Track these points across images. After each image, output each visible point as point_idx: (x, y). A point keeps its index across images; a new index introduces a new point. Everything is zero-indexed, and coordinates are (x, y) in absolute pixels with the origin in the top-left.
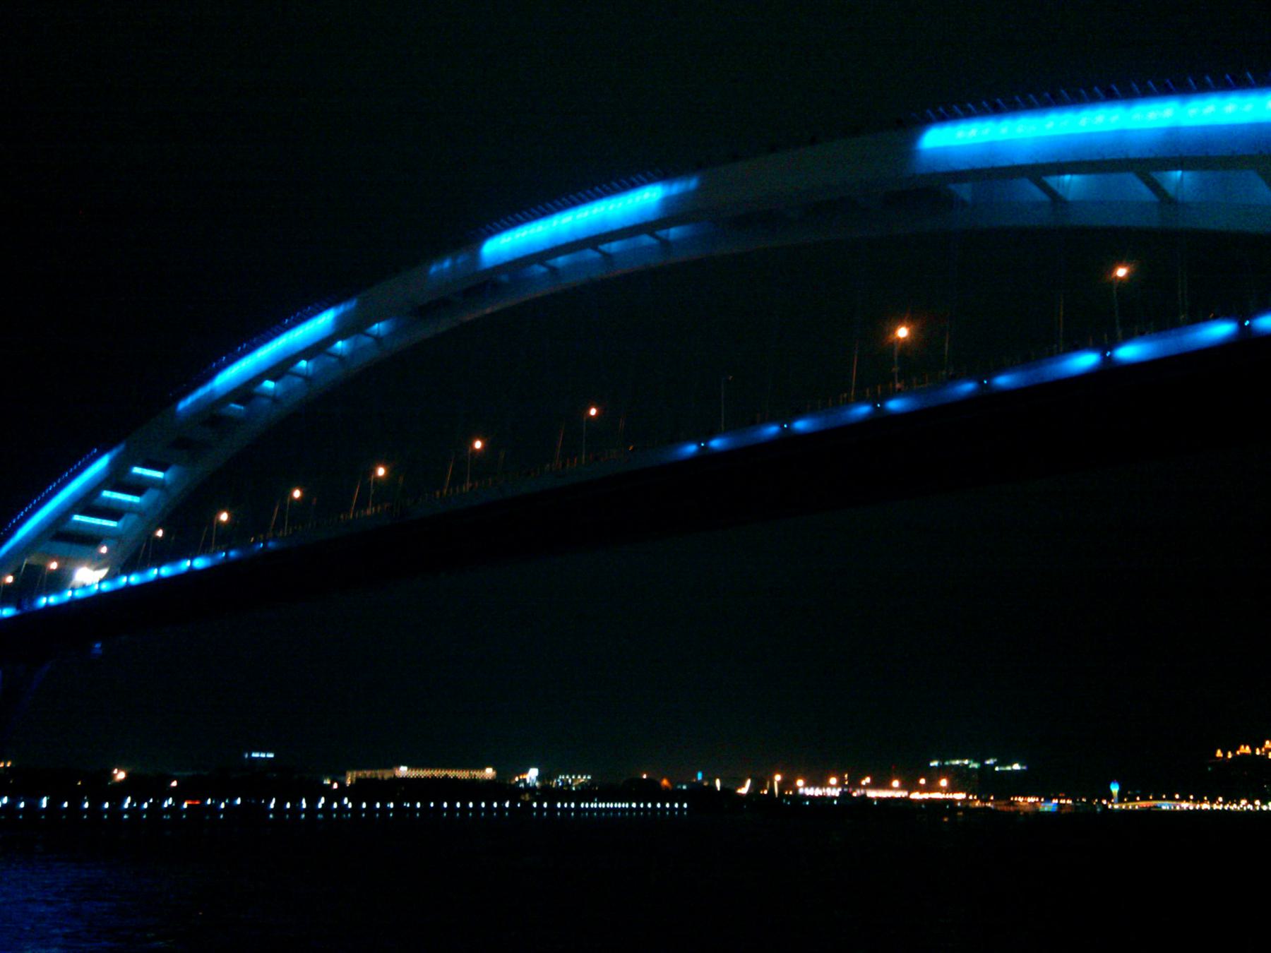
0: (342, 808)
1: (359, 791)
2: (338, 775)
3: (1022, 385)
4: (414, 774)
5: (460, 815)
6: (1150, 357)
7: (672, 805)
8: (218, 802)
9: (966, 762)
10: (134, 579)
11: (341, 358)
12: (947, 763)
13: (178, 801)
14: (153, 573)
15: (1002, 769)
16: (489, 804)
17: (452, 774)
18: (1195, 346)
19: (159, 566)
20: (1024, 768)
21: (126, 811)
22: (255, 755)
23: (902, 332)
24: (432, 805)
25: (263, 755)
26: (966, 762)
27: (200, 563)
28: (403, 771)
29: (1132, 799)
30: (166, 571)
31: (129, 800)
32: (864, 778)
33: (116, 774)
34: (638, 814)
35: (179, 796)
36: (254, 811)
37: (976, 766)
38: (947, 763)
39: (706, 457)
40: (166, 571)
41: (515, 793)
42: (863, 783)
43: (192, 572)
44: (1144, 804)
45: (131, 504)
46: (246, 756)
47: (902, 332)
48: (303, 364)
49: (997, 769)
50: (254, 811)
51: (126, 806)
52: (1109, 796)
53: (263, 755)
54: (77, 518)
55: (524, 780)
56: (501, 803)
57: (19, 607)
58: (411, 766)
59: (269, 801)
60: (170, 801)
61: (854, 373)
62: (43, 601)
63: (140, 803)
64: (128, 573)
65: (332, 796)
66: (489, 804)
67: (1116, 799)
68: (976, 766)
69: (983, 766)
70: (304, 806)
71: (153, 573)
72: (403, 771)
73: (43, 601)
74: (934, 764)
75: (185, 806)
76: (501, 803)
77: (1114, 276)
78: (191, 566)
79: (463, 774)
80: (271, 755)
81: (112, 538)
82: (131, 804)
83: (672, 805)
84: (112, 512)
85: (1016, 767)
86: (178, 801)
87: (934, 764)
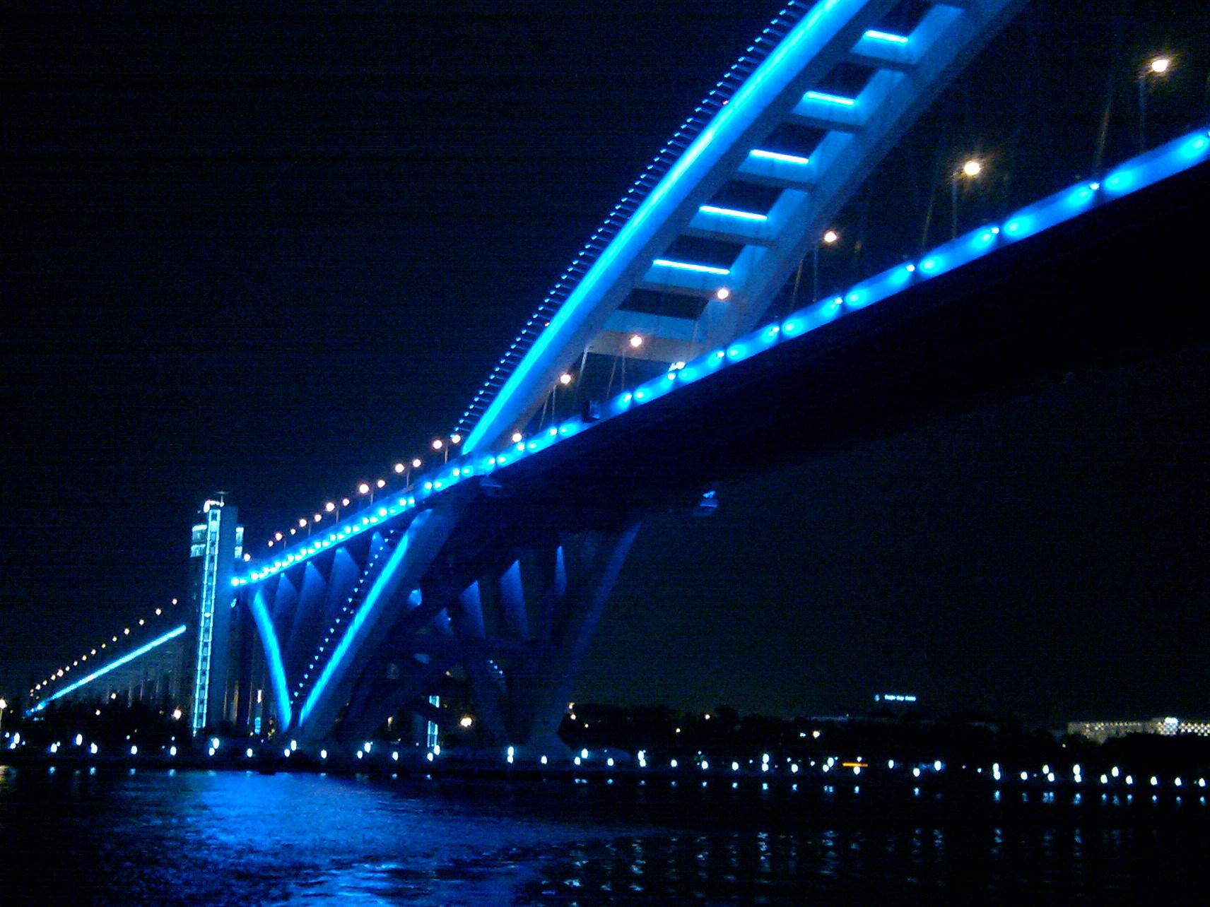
6: (948, 270)
8: (627, 756)
10: (794, 327)
14: (830, 309)
16: (1166, 781)
19: (632, 390)
23: (972, 169)
24: (964, 767)
25: (900, 698)
30: (859, 297)
33: (834, 758)
40: (859, 297)
43: (1005, 251)
45: (893, 49)
46: (877, 698)
47: (972, 169)
53: (900, 698)
56: (1189, 779)
57: (586, 418)
58: (1183, 716)
60: (585, 753)
62: (624, 401)
66: (1166, 781)
70: (997, 775)
71: (830, 309)
72: (1170, 725)
73: (624, 401)
76: (1189, 779)
77: (990, 157)
78: (780, 334)
80: (913, 699)
81: (757, 241)
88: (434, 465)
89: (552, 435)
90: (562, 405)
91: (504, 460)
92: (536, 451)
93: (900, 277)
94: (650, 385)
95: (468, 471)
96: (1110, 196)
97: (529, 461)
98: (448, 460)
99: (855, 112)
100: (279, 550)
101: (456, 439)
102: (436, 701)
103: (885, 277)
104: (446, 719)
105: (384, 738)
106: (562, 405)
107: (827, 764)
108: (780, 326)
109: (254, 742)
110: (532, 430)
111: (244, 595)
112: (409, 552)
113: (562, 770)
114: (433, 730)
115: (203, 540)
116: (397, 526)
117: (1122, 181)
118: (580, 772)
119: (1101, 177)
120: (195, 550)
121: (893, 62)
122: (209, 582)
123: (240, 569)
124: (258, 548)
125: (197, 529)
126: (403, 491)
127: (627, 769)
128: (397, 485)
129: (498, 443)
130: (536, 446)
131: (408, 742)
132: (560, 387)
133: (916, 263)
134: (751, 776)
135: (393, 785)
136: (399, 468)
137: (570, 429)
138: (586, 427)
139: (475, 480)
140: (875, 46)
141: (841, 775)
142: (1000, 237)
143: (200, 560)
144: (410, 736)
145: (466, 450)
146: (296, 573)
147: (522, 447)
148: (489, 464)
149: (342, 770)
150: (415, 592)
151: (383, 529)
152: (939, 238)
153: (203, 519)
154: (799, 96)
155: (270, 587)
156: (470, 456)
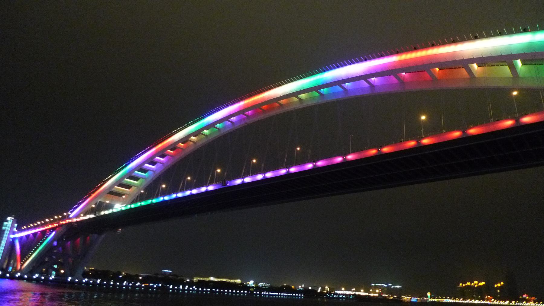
0: (193, 290)
1: (200, 284)
2: (192, 278)
3: (433, 143)
4: (216, 280)
5: (90, 286)
7: (236, 291)
9: (383, 284)
11: (206, 136)
12: (377, 285)
13: (141, 283)
15: (394, 287)
17: (228, 280)
18: (501, 128)
19: (141, 202)
20: (401, 287)
21: (124, 286)
22: (165, 271)
26: (464, 285)
27: (211, 188)
28: (212, 279)
29: (434, 298)
30: (194, 191)
31: (125, 282)
32: (124, 283)
34: (153, 289)
35: (142, 282)
36: (165, 289)
37: (386, 286)
38: (377, 285)
39: (243, 184)
41: (248, 288)
42: (352, 290)
43: (207, 192)
44: (454, 301)
48: (193, 138)
49: (392, 287)
50: (165, 289)
51: (124, 284)
52: (427, 297)
54: (136, 172)
55: (249, 284)
57: (95, 215)
58: (215, 277)
59: (170, 286)
61: (209, 179)
62: (102, 213)
63: (129, 284)
64: (131, 204)
65: (191, 284)
67: (429, 297)
68: (386, 286)
69: (388, 286)
74: (373, 285)
75: (143, 285)
79: (232, 281)
82: (126, 284)
83: (236, 291)
84: (128, 186)
85: (398, 287)
86: (141, 283)
87: (373, 285)
88: (64, 218)
89: (88, 217)
90: (92, 211)
91: (78, 220)
92: (143, 205)
93: (174, 196)
94: (169, 196)
95: (70, 221)
96: (267, 177)
97: (83, 221)
98: (209, 183)
99: (154, 168)
100: (25, 230)
101: (69, 213)
102: (56, 266)
103: (234, 181)
104: (57, 271)
105: (41, 274)
106: (92, 211)
107: (475, 301)
108: (265, 174)
109: (9, 273)
110: (85, 214)
111: (14, 239)
112: (55, 235)
113: (80, 283)
114: (54, 273)
115: (6, 226)
116: (53, 229)
117: (247, 180)
118: (84, 283)
119: (243, 178)
120: (4, 228)
121: (159, 162)
122: (6, 235)
123: (14, 233)
124: (20, 229)
125: (5, 223)
126: (56, 222)
127: (95, 284)
128: (55, 221)
129: (77, 216)
130: (85, 218)
131: (47, 275)
132: (92, 208)
133: (177, 194)
134: (178, 289)
135: (41, 284)
136: (56, 217)
137: (92, 216)
138: (95, 216)
139: (71, 223)
140: (157, 159)
141: (244, 293)
142: (288, 172)
143: (4, 230)
144: (48, 274)
145: (71, 216)
146: (28, 236)
147: (83, 218)
148: (75, 220)
149: (30, 280)
150: (56, 242)
151: (50, 229)
152: (182, 190)
153: (7, 221)
154: (144, 165)
155: (21, 239)
156: (71, 218)
